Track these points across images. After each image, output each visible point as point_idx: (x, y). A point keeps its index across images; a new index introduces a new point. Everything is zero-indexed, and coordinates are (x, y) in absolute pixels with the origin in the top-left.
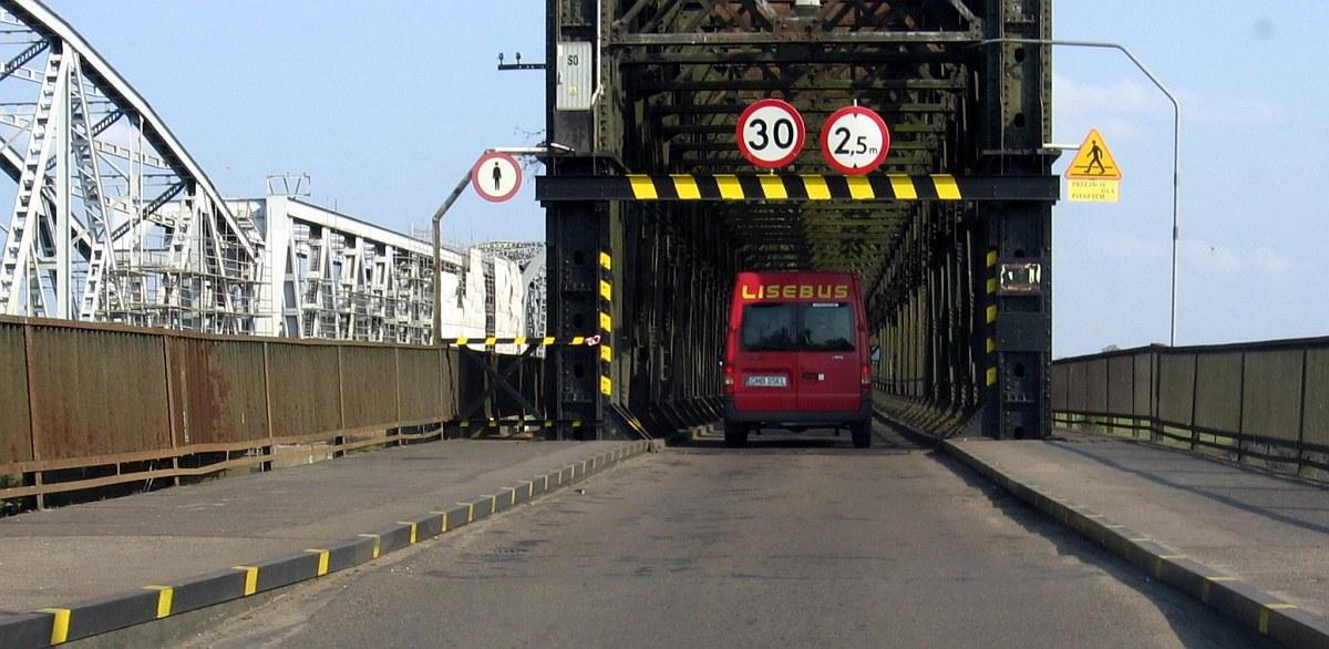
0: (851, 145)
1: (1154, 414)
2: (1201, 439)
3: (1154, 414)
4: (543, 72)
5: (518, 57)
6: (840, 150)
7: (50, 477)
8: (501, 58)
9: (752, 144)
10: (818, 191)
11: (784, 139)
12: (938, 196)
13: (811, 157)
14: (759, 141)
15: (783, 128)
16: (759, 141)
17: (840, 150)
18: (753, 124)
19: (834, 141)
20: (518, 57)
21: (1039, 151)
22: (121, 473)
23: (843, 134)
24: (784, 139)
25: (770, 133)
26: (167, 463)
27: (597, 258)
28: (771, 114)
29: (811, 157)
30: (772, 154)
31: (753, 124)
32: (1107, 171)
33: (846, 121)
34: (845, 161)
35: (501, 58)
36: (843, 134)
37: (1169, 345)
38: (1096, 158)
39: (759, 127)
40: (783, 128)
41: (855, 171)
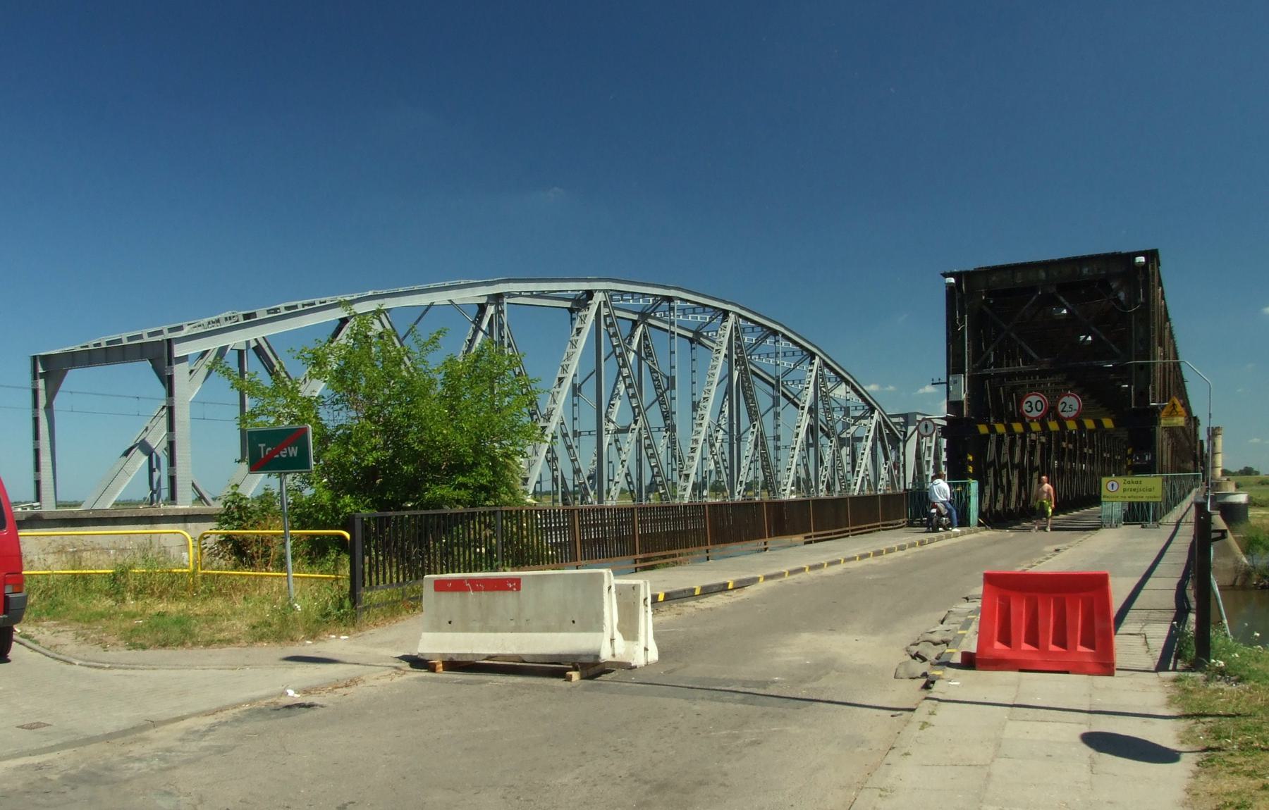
0: (1067, 409)
1: (569, 305)
2: (637, 316)
3: (383, 317)
4: (945, 385)
5: (939, 379)
6: (1062, 411)
7: (815, 536)
8: (933, 380)
9: (1026, 411)
10: (1053, 426)
11: (1039, 408)
12: (1104, 428)
13: (1051, 412)
14: (1029, 409)
15: (1039, 404)
16: (1029, 409)
17: (1062, 411)
18: (1027, 403)
19: (1060, 407)
20: (939, 379)
21: (1148, 407)
22: (711, 544)
23: (1064, 405)
24: (1039, 408)
25: (1033, 406)
26: (810, 537)
27: (973, 458)
28: (1033, 399)
29: (1051, 412)
30: (1035, 414)
31: (1027, 403)
32: (1179, 414)
33: (1065, 399)
34: (1065, 415)
35: (933, 380)
36: (1064, 405)
37: (1175, 591)
38: (1174, 409)
39: (1029, 404)
40: (1039, 404)
41: (1069, 419)
